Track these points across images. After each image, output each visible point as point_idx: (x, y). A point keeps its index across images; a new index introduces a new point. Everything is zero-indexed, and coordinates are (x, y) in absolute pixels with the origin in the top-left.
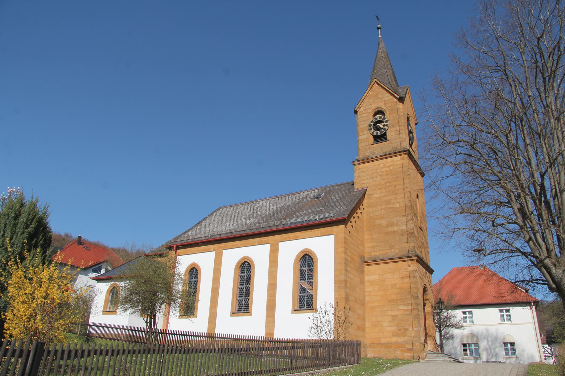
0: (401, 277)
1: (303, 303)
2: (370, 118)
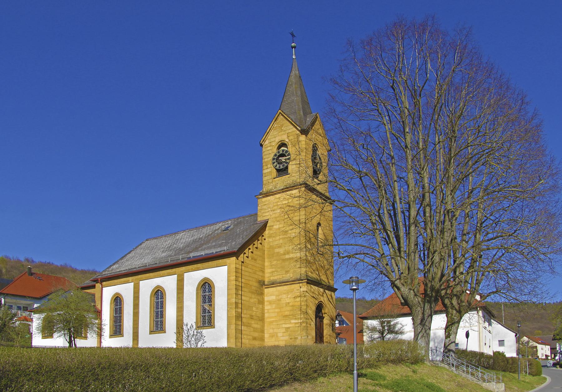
0: (293, 297)
1: (209, 321)
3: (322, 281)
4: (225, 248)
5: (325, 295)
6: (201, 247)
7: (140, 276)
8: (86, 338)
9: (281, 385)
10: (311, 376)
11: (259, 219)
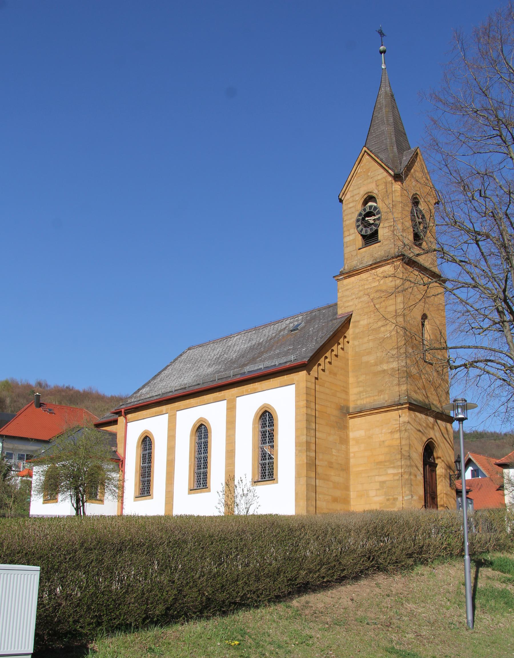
0: (390, 431)
1: (204, 481)
2: (358, 209)
3: (432, 406)
4: (292, 358)
5: (436, 428)
6: (261, 357)
7: (177, 404)
8: (101, 501)
9: (357, 578)
10: (403, 563)
11: (340, 312)
